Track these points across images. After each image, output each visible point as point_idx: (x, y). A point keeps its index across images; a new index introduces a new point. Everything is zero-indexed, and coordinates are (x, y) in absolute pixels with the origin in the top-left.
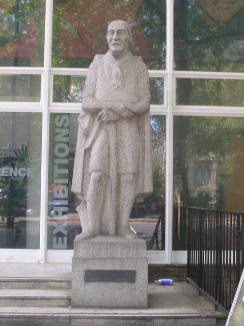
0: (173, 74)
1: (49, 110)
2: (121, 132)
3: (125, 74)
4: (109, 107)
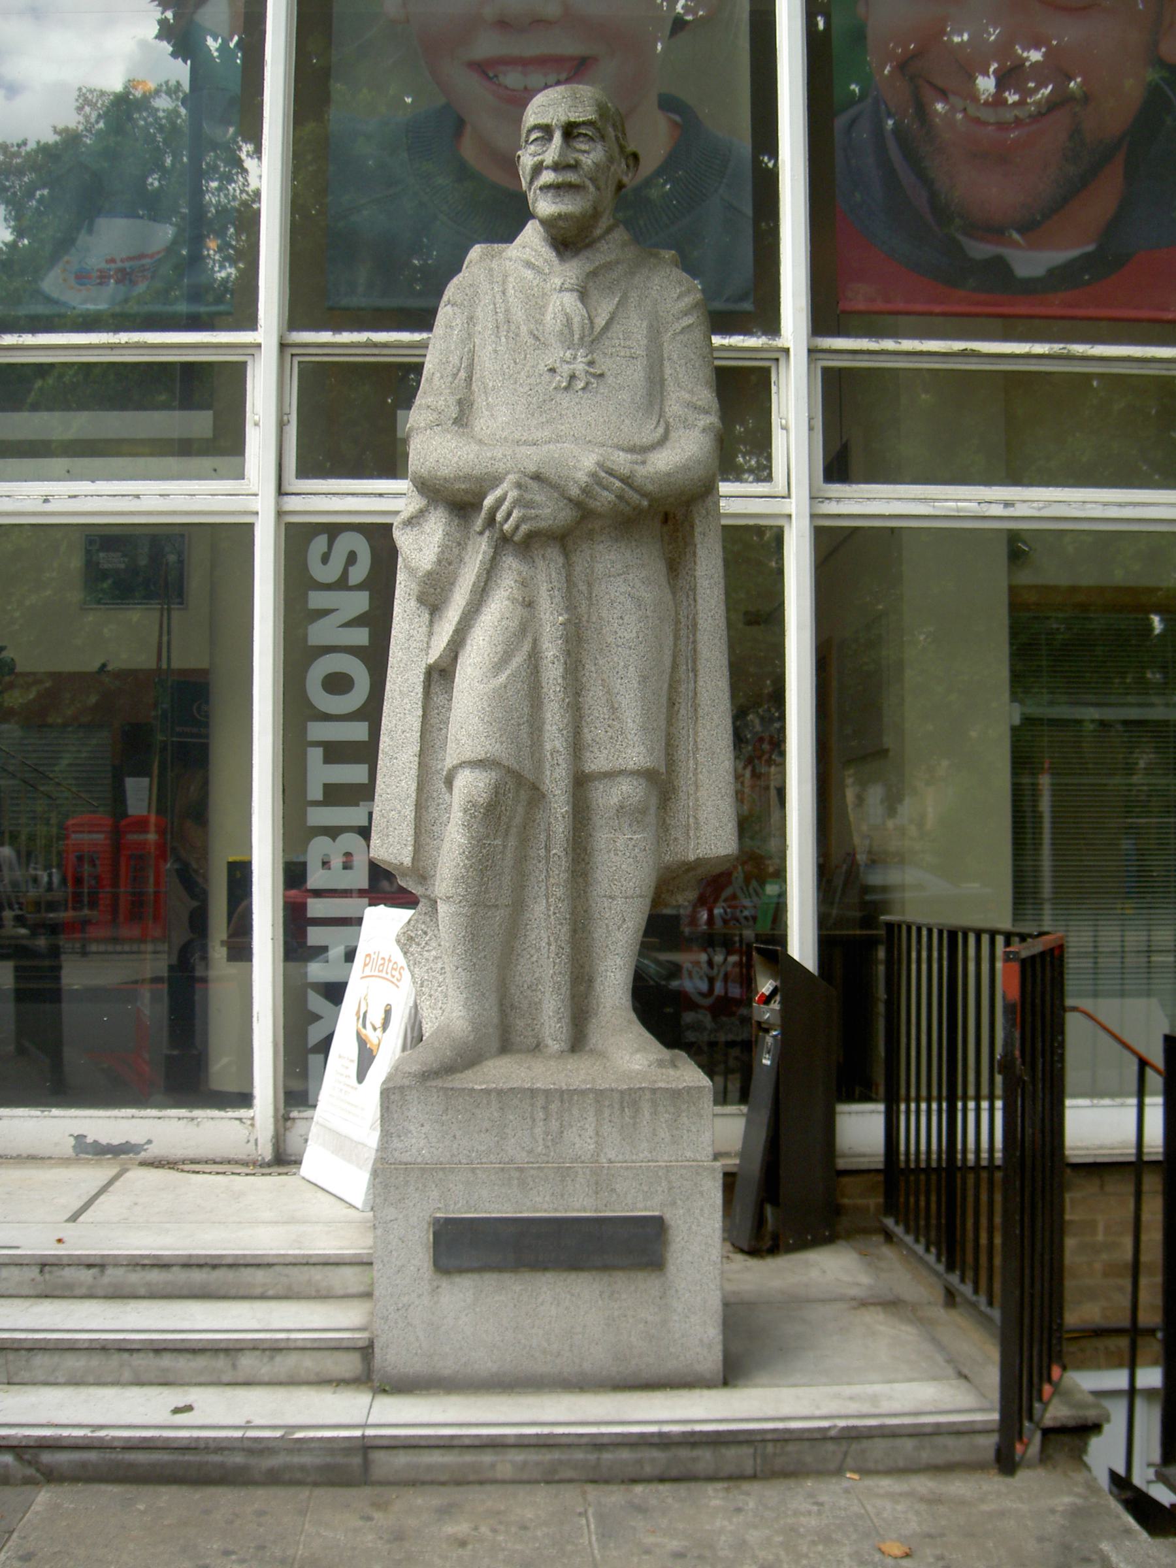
0: (811, 351)
1: (280, 514)
2: (590, 585)
3: (600, 322)
4: (532, 468)
